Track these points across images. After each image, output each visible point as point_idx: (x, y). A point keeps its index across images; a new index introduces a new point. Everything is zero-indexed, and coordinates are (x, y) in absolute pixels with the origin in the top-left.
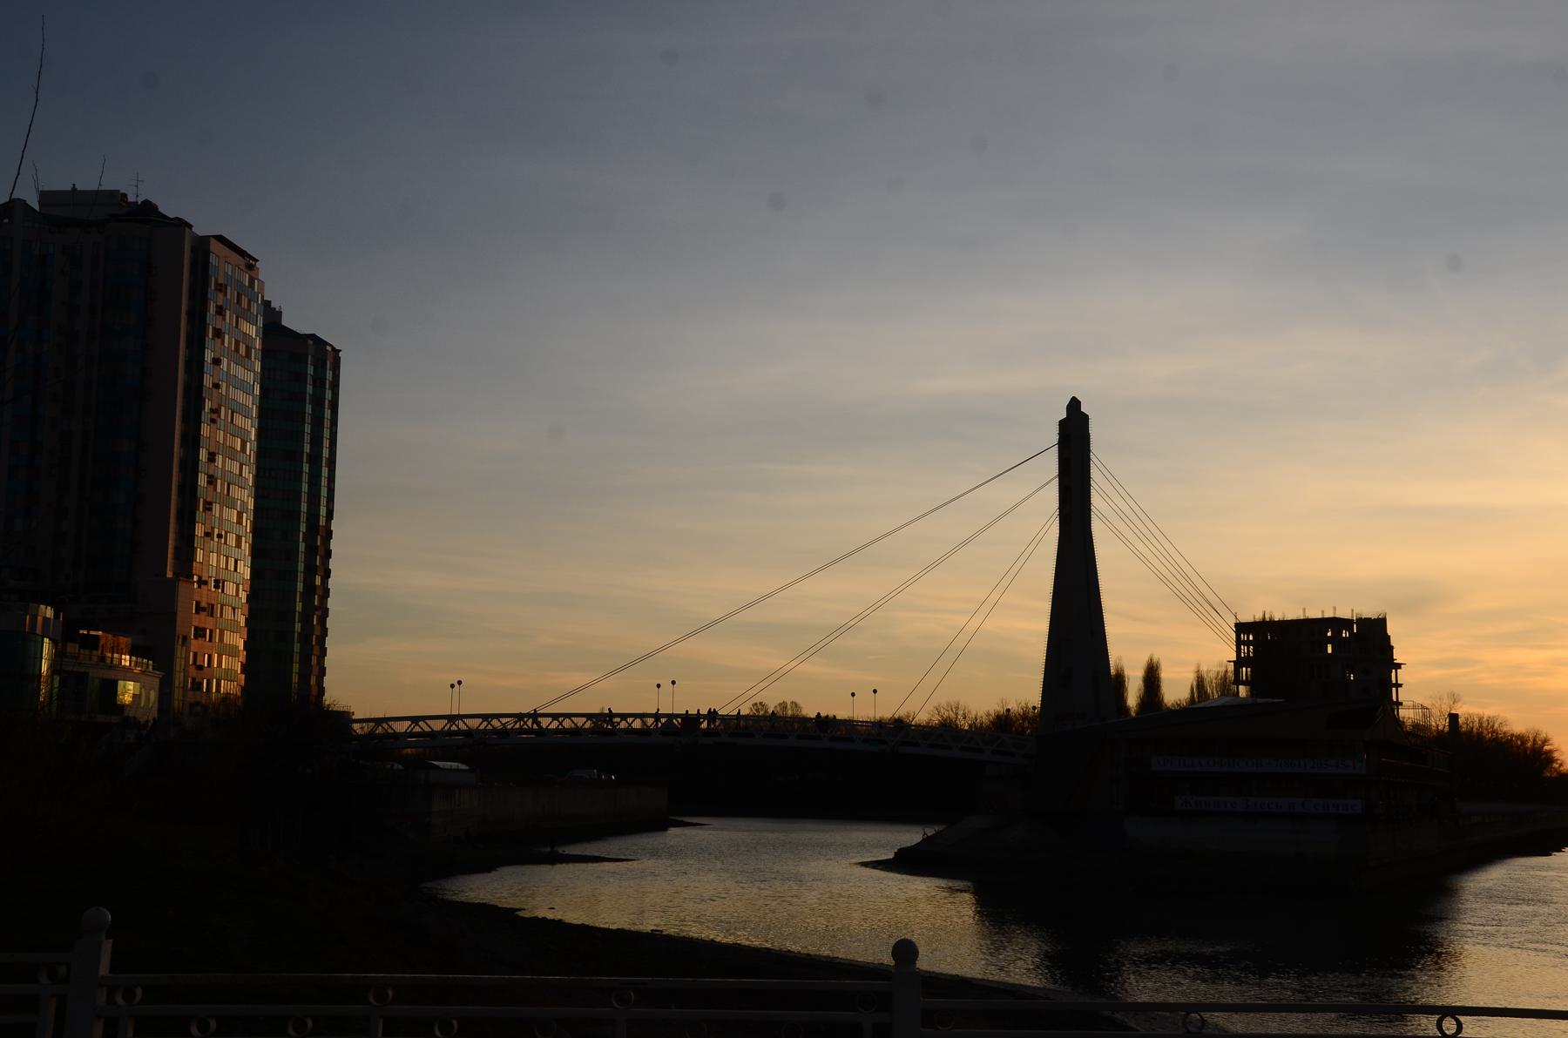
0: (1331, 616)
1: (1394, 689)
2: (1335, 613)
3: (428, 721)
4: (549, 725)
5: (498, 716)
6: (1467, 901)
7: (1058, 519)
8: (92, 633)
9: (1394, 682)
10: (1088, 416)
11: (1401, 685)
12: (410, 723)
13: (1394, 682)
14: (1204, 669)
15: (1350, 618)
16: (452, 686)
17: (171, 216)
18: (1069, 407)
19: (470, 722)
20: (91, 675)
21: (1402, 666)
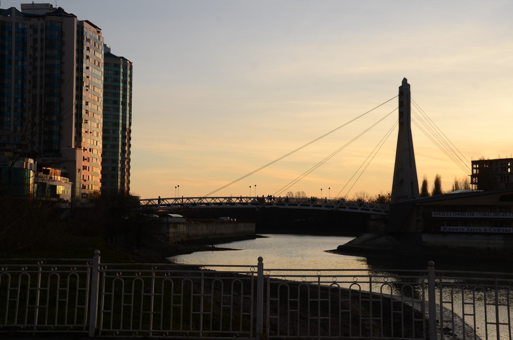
2: (511, 156)
16: (176, 187)
19: (194, 200)
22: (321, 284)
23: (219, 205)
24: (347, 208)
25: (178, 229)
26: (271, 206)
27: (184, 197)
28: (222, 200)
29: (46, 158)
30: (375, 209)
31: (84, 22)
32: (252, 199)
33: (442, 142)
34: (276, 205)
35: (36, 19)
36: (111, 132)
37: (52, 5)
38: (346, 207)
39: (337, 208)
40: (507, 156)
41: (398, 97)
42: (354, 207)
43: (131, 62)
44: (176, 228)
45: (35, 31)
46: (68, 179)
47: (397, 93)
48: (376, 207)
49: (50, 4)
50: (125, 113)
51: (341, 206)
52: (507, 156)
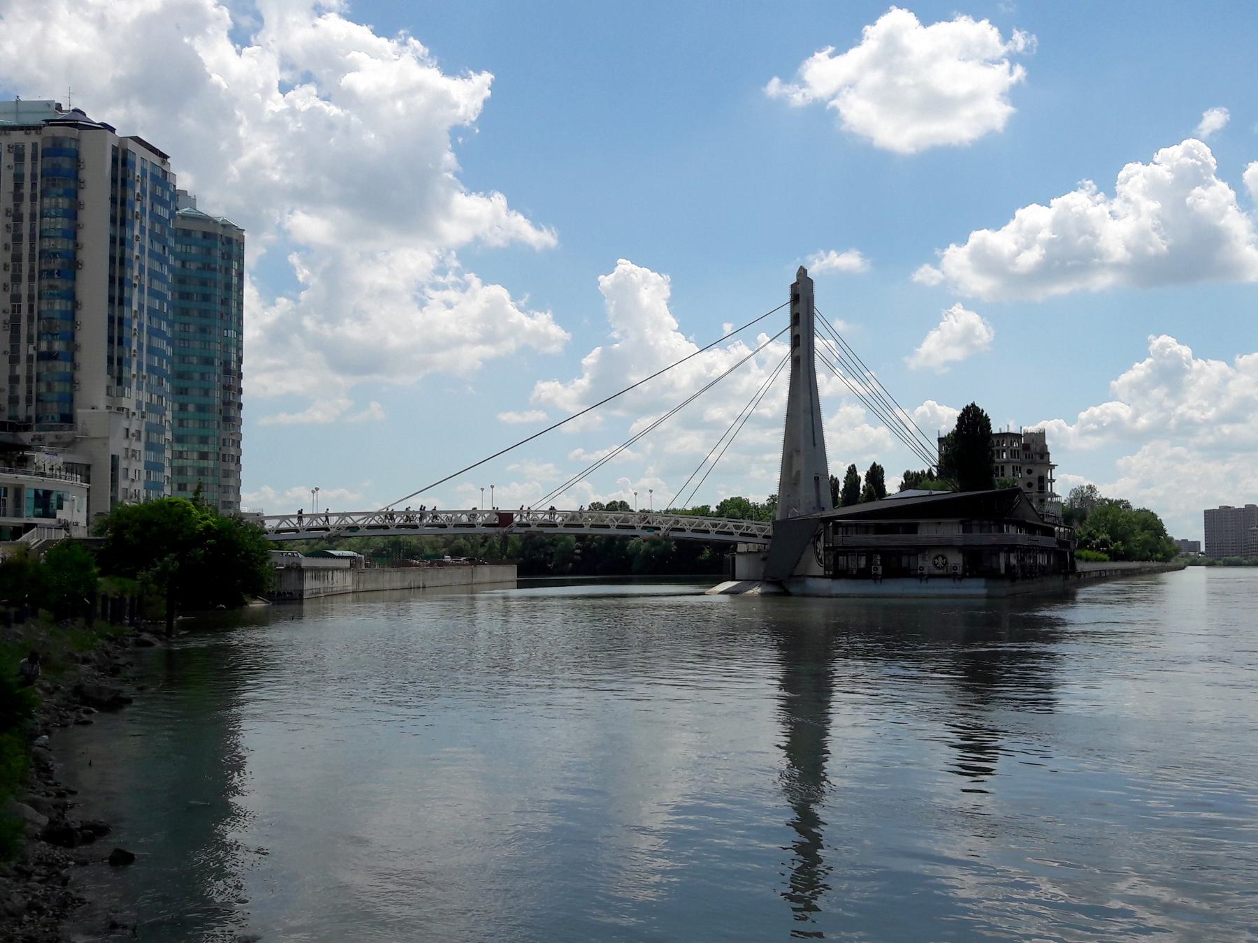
0: (1006, 431)
1: (1049, 484)
2: (1009, 430)
3: (352, 517)
4: (358, 521)
5: (349, 515)
6: (1173, 154)
7: (790, 359)
8: (875, 494)
9: (1049, 478)
10: (812, 280)
11: (1054, 481)
12: (338, 518)
13: (1049, 478)
14: (876, 463)
15: (1019, 433)
16: (313, 492)
17: (497, 285)
18: (799, 275)
19: (356, 518)
20: (26, 486)
21: (1056, 467)
22: (1049, 484)
23: (487, 527)
24: (711, 533)
25: (328, 582)
26: (526, 529)
27: (329, 512)
28: (356, 518)
29: (42, 433)
30: (745, 531)
31: (129, 139)
32: (487, 515)
33: (913, 448)
34: (616, 528)
35: (22, 132)
36: (197, 376)
37: (60, 104)
38: (710, 529)
39: (667, 530)
40: (1000, 429)
41: (788, 307)
42: (725, 529)
43: (240, 227)
44: (324, 580)
45: (19, 157)
46: (79, 476)
47: (787, 297)
48: (748, 528)
49: (56, 102)
50: (1140, 569)
51: (676, 527)
52: (1000, 429)
